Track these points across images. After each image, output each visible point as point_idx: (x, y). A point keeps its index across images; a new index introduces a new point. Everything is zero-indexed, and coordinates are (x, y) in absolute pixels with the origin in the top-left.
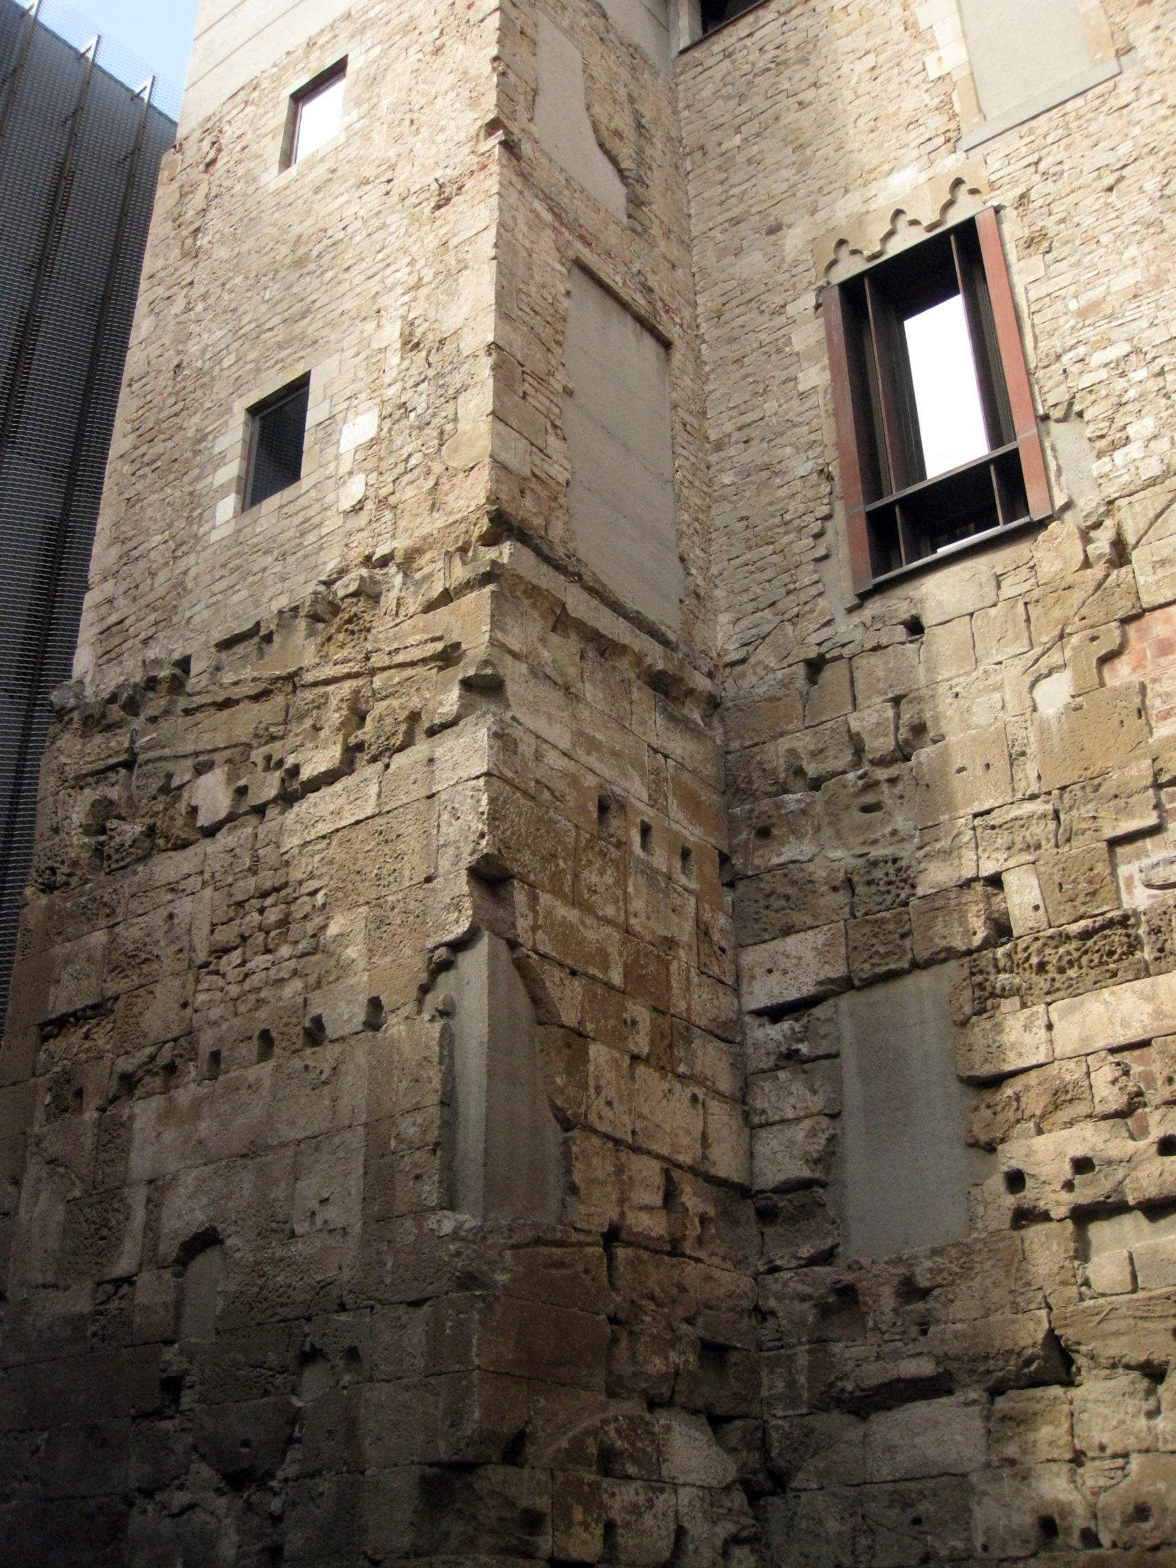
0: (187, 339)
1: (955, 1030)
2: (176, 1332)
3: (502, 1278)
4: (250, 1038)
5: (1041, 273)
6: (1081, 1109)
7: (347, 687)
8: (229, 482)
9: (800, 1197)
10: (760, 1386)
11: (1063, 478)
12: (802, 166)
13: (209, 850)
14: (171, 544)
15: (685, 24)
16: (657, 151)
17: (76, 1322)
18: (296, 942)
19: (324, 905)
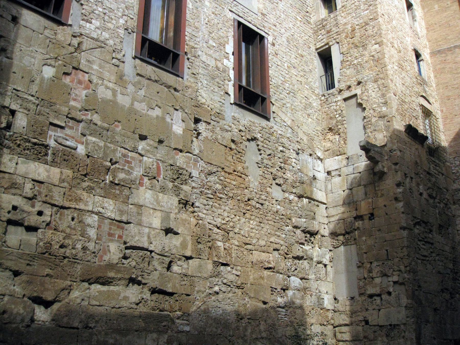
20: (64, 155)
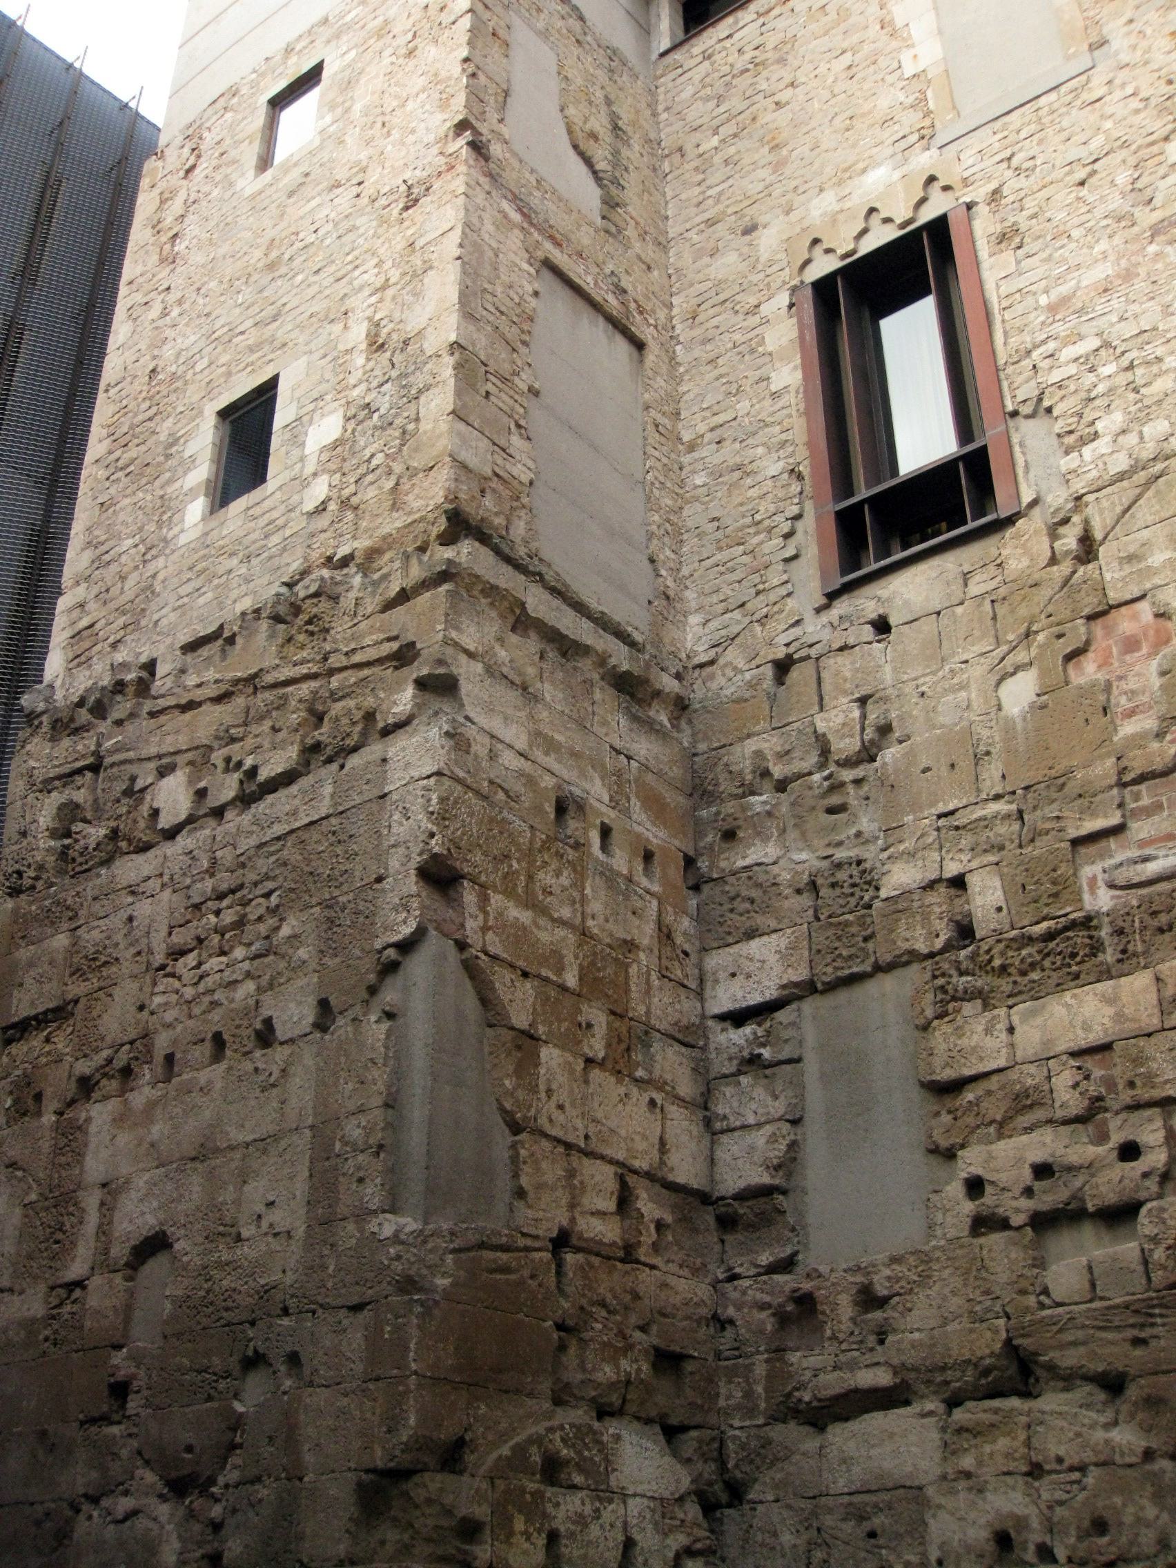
0: (165, 345)
1: (917, 1034)
2: (126, 1335)
3: (442, 1282)
4: (203, 1040)
5: (1013, 268)
6: (1040, 1114)
7: (305, 689)
8: (199, 484)
9: (760, 1204)
10: (718, 1395)
11: (1031, 475)
12: (778, 166)
13: (169, 852)
14: (142, 548)
15: (666, 23)
16: (634, 153)
17: (30, 1325)
18: (250, 945)
19: (278, 906)
20: (1154, 914)
